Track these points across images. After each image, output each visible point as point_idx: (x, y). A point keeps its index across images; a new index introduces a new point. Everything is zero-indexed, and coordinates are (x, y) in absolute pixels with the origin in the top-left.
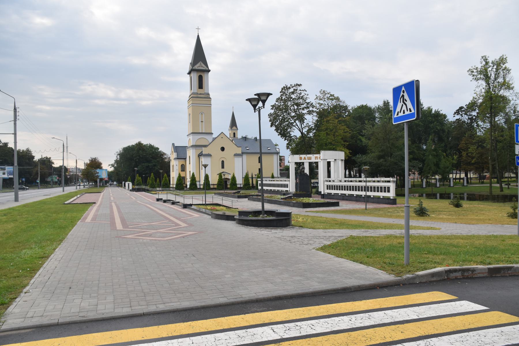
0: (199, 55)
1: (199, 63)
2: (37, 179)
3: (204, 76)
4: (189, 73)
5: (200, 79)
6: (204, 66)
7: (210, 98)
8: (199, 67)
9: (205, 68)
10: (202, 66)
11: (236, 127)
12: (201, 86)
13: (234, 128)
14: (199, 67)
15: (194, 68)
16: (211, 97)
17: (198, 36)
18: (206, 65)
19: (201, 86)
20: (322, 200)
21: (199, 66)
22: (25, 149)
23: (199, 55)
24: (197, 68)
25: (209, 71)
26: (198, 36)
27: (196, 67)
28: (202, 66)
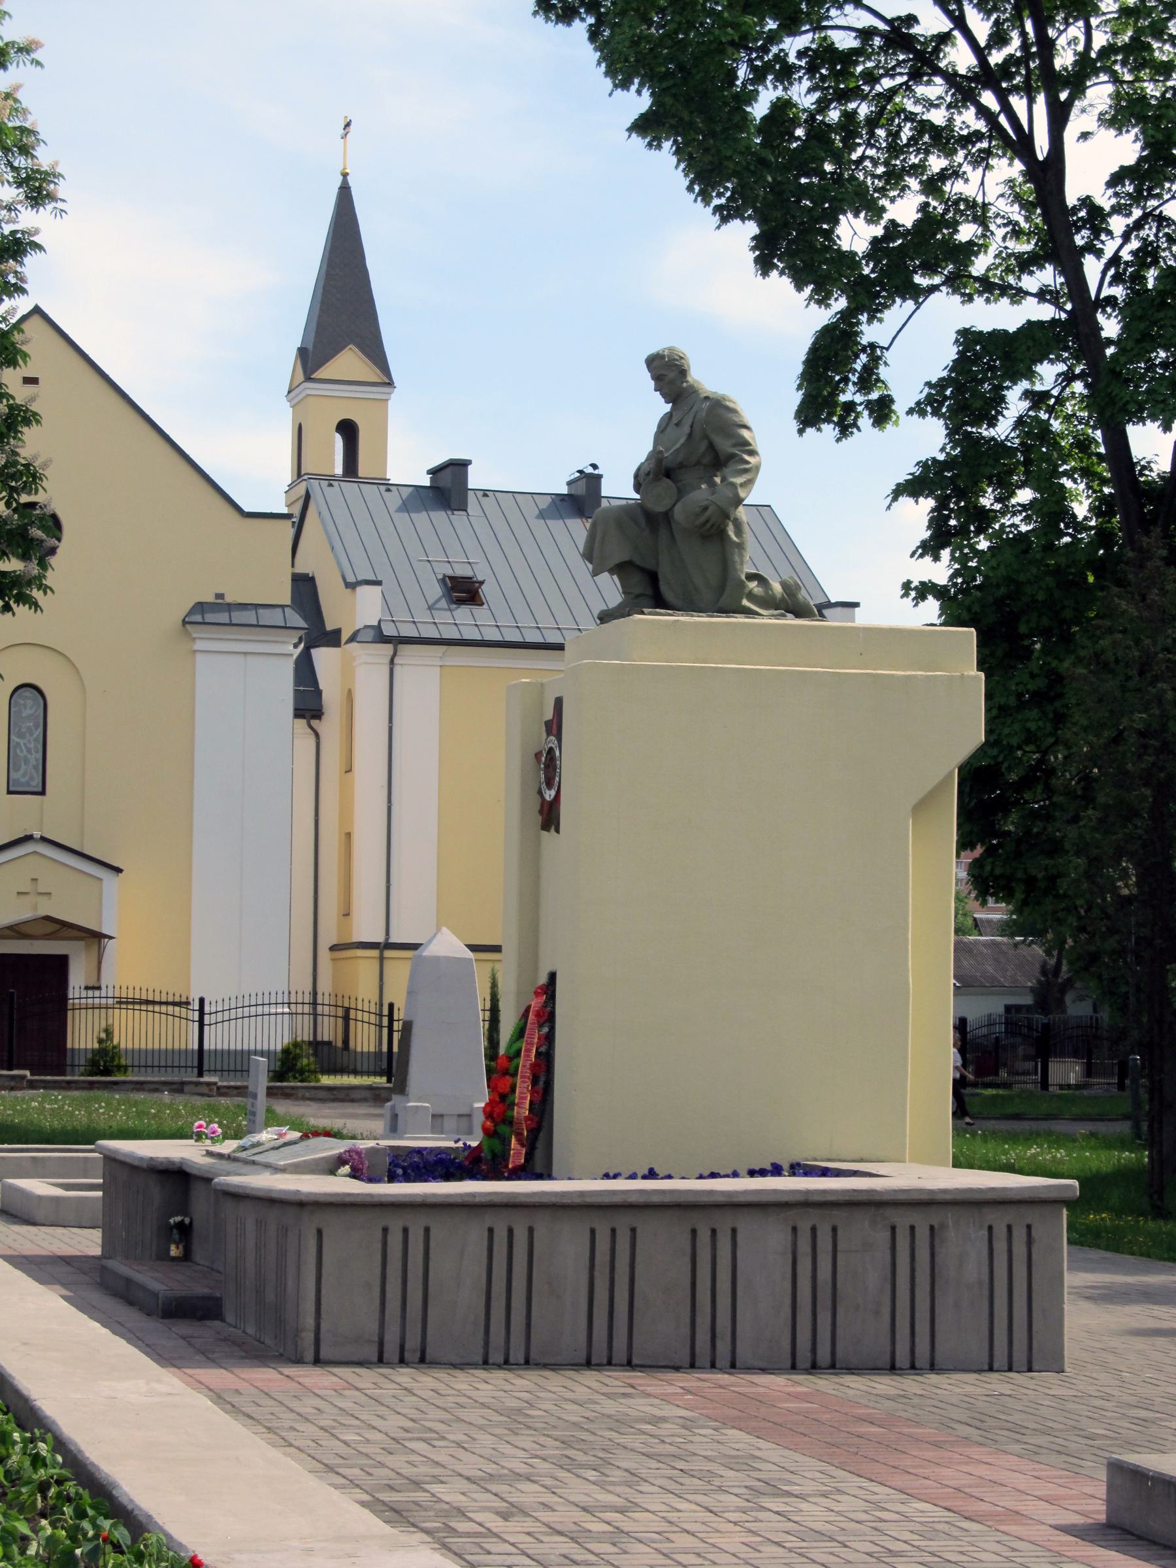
11: (376, 354)
13: (349, 363)
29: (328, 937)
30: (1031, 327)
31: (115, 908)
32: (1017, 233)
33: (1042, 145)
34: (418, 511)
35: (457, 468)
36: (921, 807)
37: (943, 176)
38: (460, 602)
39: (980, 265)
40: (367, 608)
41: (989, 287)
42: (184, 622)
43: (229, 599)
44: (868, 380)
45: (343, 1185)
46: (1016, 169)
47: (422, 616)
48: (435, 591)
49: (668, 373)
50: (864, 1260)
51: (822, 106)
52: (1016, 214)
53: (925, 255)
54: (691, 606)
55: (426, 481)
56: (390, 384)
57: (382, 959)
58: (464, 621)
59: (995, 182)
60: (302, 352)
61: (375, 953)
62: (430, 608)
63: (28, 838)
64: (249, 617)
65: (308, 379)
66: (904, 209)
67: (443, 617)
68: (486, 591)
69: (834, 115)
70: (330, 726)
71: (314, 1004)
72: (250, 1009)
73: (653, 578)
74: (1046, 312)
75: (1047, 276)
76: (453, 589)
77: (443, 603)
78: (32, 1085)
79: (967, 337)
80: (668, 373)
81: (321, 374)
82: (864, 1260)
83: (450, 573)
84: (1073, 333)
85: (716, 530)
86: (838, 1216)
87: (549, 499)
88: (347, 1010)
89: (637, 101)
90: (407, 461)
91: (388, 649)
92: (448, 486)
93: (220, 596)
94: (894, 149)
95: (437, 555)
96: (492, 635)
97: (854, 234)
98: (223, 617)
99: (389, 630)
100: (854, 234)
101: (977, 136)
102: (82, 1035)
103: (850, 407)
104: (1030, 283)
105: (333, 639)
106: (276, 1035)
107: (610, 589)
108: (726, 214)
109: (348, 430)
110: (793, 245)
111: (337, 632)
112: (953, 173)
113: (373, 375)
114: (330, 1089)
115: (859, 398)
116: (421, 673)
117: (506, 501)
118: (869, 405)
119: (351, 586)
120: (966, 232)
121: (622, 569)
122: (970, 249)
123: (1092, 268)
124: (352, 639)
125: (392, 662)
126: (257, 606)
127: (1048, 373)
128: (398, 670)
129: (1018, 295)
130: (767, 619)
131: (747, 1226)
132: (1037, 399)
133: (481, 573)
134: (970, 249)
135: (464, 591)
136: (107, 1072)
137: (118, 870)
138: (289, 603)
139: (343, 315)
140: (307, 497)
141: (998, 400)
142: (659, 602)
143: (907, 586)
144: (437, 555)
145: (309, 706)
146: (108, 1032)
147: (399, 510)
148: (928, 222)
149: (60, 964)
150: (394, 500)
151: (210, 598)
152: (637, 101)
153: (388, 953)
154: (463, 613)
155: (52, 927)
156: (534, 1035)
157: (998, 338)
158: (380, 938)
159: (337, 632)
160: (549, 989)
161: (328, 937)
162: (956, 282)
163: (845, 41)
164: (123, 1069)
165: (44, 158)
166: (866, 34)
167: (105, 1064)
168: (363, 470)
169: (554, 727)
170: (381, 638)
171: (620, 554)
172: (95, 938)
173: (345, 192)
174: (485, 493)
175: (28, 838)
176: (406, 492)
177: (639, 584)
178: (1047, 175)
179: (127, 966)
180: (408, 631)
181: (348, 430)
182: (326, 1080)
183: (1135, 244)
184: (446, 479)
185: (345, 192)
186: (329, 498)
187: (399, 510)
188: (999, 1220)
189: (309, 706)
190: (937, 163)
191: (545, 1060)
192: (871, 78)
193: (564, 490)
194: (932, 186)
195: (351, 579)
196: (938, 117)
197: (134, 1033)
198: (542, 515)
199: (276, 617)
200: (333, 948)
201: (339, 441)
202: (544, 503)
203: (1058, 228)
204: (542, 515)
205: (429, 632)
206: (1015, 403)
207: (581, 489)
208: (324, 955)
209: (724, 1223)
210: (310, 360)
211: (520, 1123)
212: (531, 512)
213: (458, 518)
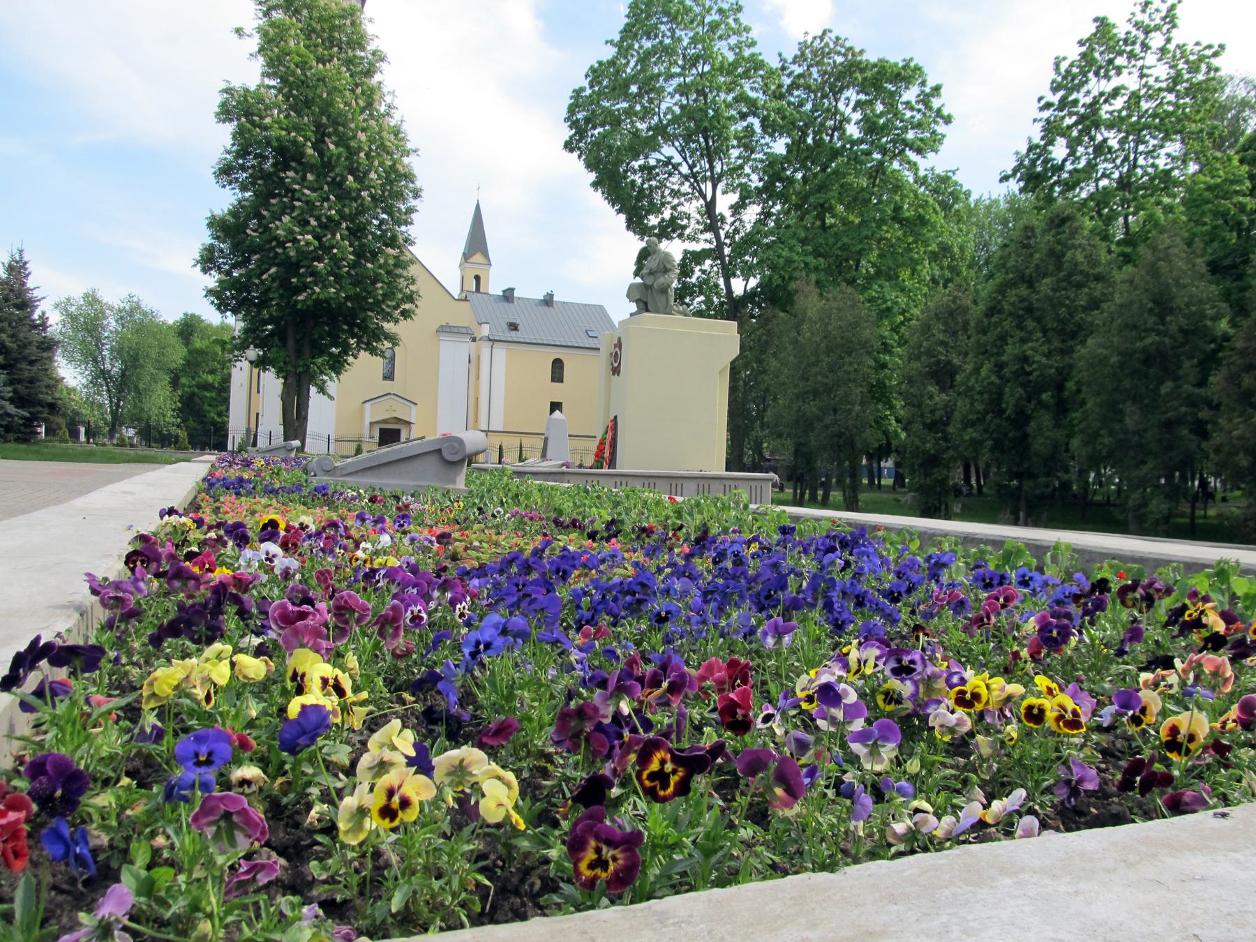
11: (486, 255)
13: (478, 258)
30: (703, 250)
32: (698, 223)
33: (709, 199)
35: (512, 290)
36: (721, 372)
37: (678, 205)
39: (687, 231)
41: (692, 238)
46: (702, 202)
48: (505, 327)
51: (643, 183)
52: (699, 217)
53: (671, 228)
54: (657, 311)
58: (514, 336)
59: (693, 207)
66: (667, 214)
69: (646, 186)
73: (646, 304)
74: (707, 246)
75: (708, 236)
79: (686, 252)
84: (716, 253)
86: (711, 482)
89: (593, 176)
90: (495, 287)
92: (508, 295)
94: (663, 197)
97: (653, 220)
100: (653, 220)
101: (688, 194)
104: (703, 237)
107: (633, 307)
108: (619, 211)
109: (477, 278)
110: (636, 223)
112: (680, 204)
116: (501, 352)
120: (685, 222)
121: (637, 301)
122: (684, 227)
123: (722, 233)
127: (708, 262)
129: (698, 241)
130: (679, 317)
132: (704, 272)
134: (684, 227)
135: (514, 327)
139: (477, 244)
141: (693, 272)
142: (647, 310)
148: (673, 219)
149: (398, 432)
152: (593, 176)
156: (610, 434)
157: (693, 253)
162: (680, 236)
163: (652, 162)
165: (418, 184)
166: (658, 161)
168: (482, 290)
171: (638, 297)
172: (408, 423)
173: (478, 206)
177: (642, 306)
178: (710, 206)
181: (477, 278)
184: (508, 294)
185: (478, 206)
190: (676, 201)
192: (657, 174)
194: (674, 208)
196: (676, 187)
203: (712, 221)
206: (697, 274)
210: (466, 256)
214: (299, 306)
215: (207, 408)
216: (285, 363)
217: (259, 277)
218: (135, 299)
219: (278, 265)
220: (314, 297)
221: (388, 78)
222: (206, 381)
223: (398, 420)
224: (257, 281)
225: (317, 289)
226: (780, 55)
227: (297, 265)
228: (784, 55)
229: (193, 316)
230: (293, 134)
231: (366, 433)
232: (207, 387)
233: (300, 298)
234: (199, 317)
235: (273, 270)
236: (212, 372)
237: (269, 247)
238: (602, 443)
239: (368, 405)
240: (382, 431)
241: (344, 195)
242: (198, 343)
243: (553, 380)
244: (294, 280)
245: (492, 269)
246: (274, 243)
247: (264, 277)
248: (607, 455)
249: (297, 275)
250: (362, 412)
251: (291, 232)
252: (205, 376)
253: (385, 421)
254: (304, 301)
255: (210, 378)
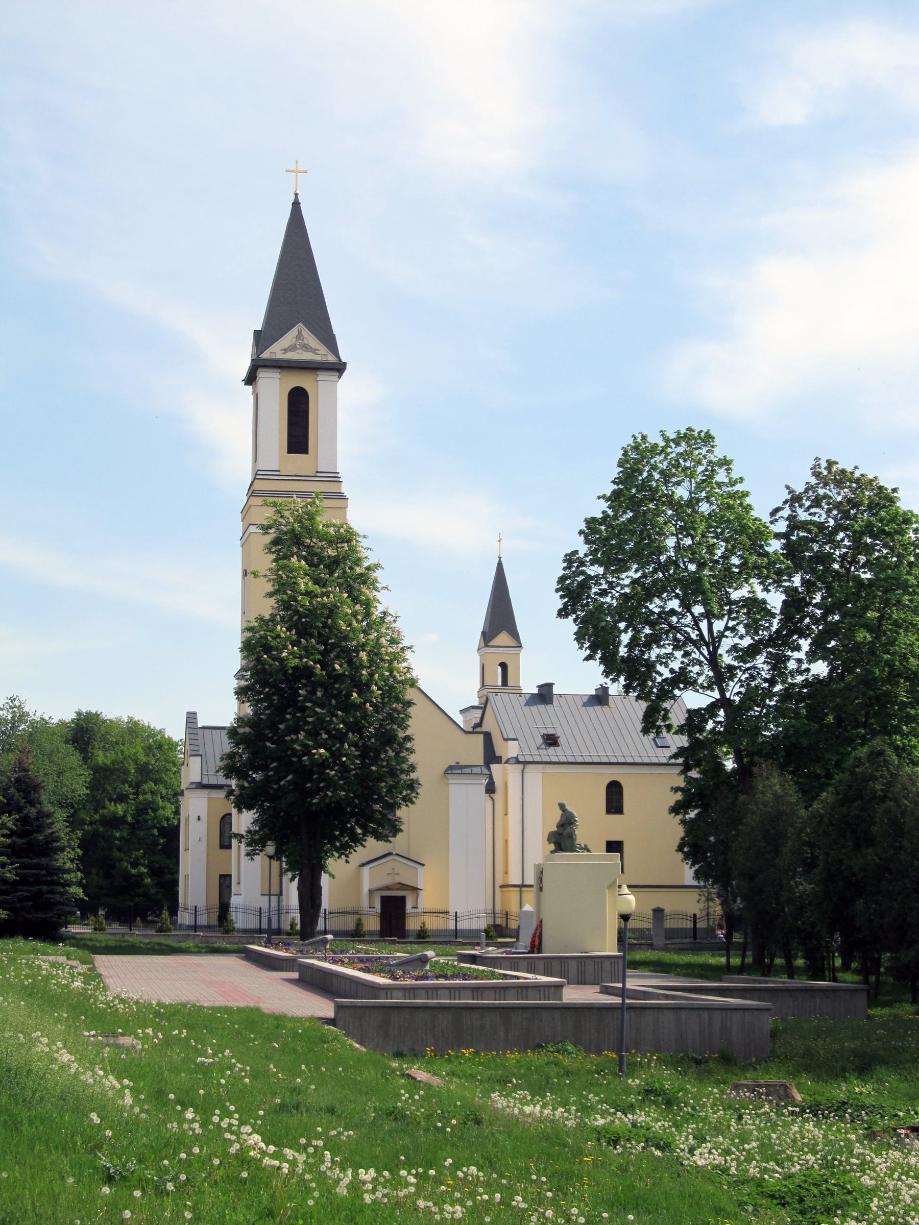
0: (297, 293)
1: (293, 332)
2: (784, 718)
3: (319, 388)
4: (251, 379)
5: (298, 405)
6: (312, 341)
7: (342, 497)
8: (293, 348)
9: (322, 355)
10: (306, 347)
11: (515, 635)
12: (298, 439)
13: (503, 638)
14: (293, 348)
15: (266, 355)
16: (345, 489)
17: (296, 205)
18: (330, 341)
19: (298, 439)
20: (894, 1011)
21: (294, 343)
22: (74, 716)
23: (297, 293)
24: (280, 356)
25: (339, 368)
26: (296, 205)
27: (276, 351)
28: (306, 347)
29: (499, 882)
31: (424, 879)
34: (532, 705)
38: (550, 745)
40: (511, 750)
42: (445, 773)
43: (461, 764)
44: (665, 718)
45: (504, 955)
47: (535, 752)
48: (540, 741)
49: (562, 807)
50: (590, 968)
55: (536, 691)
56: (521, 647)
57: (521, 891)
58: (552, 753)
60: (483, 633)
61: (518, 889)
62: (538, 748)
63: (390, 854)
64: (468, 771)
65: (486, 646)
67: (543, 752)
68: (561, 740)
70: (498, 796)
71: (494, 913)
72: (474, 916)
73: (560, 844)
76: (548, 739)
77: (543, 746)
78: (399, 943)
80: (562, 807)
81: (491, 644)
82: (590, 968)
83: (546, 732)
85: (571, 837)
87: (587, 697)
88: (507, 914)
90: (530, 687)
91: (521, 766)
92: (545, 695)
93: (458, 763)
95: (540, 725)
96: (563, 759)
98: (459, 771)
99: (521, 759)
102: (412, 925)
103: (660, 727)
105: (498, 760)
106: (481, 924)
107: (552, 847)
109: (504, 666)
111: (501, 757)
113: (512, 642)
114: (501, 943)
115: (663, 724)
116: (534, 775)
117: (569, 699)
118: (665, 726)
119: (506, 740)
121: (555, 843)
124: (507, 762)
125: (523, 771)
126: (471, 766)
128: (525, 775)
131: (571, 962)
133: (559, 733)
135: (551, 741)
136: (423, 938)
137: (423, 865)
138: (482, 764)
140: (487, 700)
143: (672, 788)
144: (540, 725)
145: (490, 789)
146: (424, 924)
147: (525, 705)
149: (402, 900)
150: (523, 700)
151: (454, 764)
153: (524, 889)
154: (551, 750)
155: (399, 886)
158: (519, 882)
159: (501, 757)
160: (541, 921)
161: (499, 882)
164: (429, 937)
167: (422, 936)
169: (542, 873)
170: (518, 762)
172: (415, 889)
174: (561, 696)
175: (390, 854)
176: (528, 697)
179: (427, 900)
180: (529, 759)
181: (504, 666)
182: (500, 940)
183: (747, 675)
184: (544, 692)
186: (497, 701)
187: (525, 705)
188: (612, 960)
189: (490, 789)
191: (541, 934)
193: (594, 693)
195: (506, 737)
197: (432, 924)
198: (585, 705)
199: (477, 770)
200: (501, 887)
201: (500, 670)
202: (585, 699)
204: (585, 705)
205: (537, 759)
207: (600, 693)
208: (498, 889)
209: (566, 960)
210: (487, 637)
211: (536, 945)
212: (580, 703)
213: (549, 707)
214: (314, 808)
215: (116, 854)
216: (301, 857)
217: (277, 783)
218: (17, 703)
219: (295, 772)
220: (327, 801)
221: (385, 601)
222: (114, 815)
223: (403, 886)
224: (275, 786)
225: (329, 793)
226: (787, 487)
227: (311, 773)
228: (793, 487)
229: (89, 714)
230: (305, 660)
231: (365, 903)
232: (115, 822)
233: (315, 801)
234: (97, 715)
235: (290, 777)
236: (122, 798)
237: (287, 760)
238: (534, 936)
239: (366, 869)
240: (384, 899)
241: (348, 707)
242: (101, 758)
243: (609, 811)
244: (308, 785)
245: (523, 654)
246: (289, 753)
247: (282, 783)
248: (537, 943)
249: (311, 780)
250: (358, 877)
251: (305, 746)
252: (112, 807)
253: (388, 888)
254: (317, 804)
255: (120, 809)
